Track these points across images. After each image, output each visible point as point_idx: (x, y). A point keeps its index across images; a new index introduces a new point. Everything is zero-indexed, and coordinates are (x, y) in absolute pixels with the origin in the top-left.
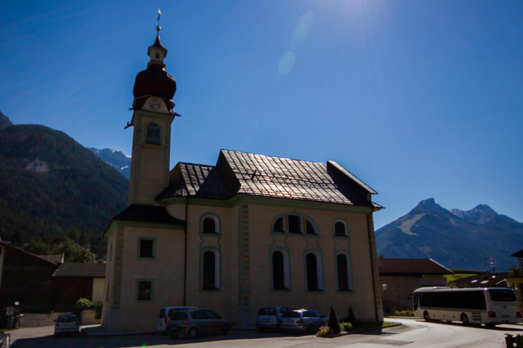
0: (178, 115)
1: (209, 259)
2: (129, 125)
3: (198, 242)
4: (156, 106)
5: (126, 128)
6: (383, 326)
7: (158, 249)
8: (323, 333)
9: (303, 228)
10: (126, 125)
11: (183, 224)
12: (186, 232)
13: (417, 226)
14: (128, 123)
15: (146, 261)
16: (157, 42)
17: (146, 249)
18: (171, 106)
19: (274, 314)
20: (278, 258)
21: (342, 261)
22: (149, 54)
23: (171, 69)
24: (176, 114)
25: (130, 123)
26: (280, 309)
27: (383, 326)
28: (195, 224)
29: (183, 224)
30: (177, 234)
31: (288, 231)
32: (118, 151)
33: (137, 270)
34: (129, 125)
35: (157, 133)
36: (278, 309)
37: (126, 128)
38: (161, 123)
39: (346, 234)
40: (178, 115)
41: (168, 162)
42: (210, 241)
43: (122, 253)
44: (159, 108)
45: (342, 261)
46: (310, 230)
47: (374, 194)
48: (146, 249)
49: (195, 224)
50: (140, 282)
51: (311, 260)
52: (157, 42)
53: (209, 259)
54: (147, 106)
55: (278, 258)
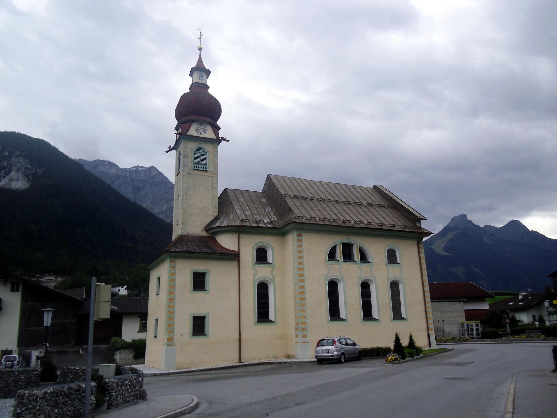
0: (225, 140)
1: (263, 290)
2: (170, 149)
3: (252, 273)
5: (167, 152)
6: (238, 251)
7: (211, 281)
9: (356, 256)
11: (234, 256)
14: (170, 147)
16: (200, 61)
18: (216, 129)
19: (333, 345)
20: (333, 286)
21: (394, 286)
22: (191, 75)
23: (216, 88)
24: (223, 139)
26: (339, 340)
27: (238, 251)
28: (248, 254)
33: (191, 304)
34: (170, 149)
36: (336, 339)
37: (167, 152)
39: (398, 261)
40: (225, 140)
41: (216, 189)
42: (263, 272)
43: (174, 287)
45: (394, 286)
46: (363, 258)
47: (423, 219)
51: (365, 287)
52: (200, 61)
53: (263, 290)
54: (193, 131)
55: (333, 286)
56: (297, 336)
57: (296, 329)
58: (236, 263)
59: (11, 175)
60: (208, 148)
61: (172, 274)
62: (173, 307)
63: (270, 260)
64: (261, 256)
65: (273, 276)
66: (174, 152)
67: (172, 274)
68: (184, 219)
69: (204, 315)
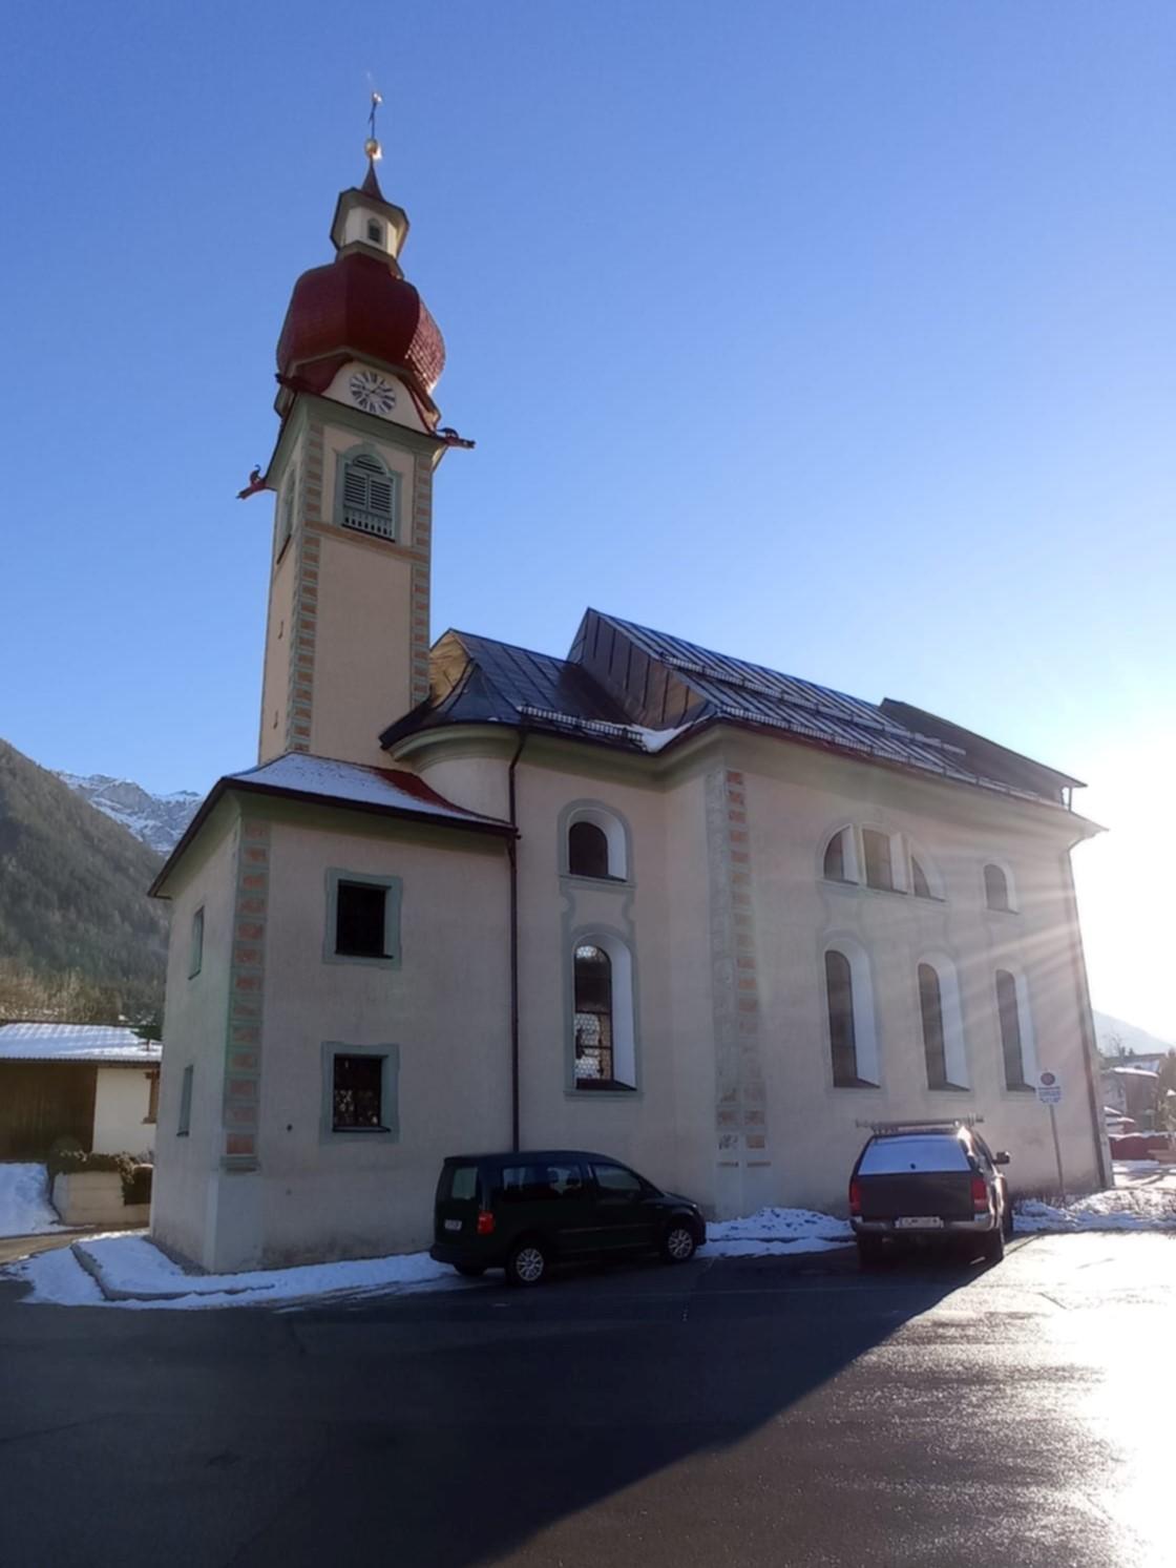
2: (259, 483)
4: (376, 400)
5: (244, 494)
7: (404, 920)
8: (1011, 1219)
10: (247, 484)
12: (513, 864)
13: (1028, 1480)
14: (254, 475)
15: (358, 971)
17: (361, 920)
25: (262, 475)
28: (544, 843)
29: (499, 837)
30: (482, 874)
31: (865, 880)
32: (129, 781)
34: (259, 483)
35: (382, 497)
37: (244, 494)
38: (396, 460)
42: (594, 902)
43: (259, 932)
44: (389, 407)
48: (361, 920)
49: (544, 843)
50: (339, 1060)
52: (371, 179)
54: (343, 387)
56: (725, 1143)
57: (724, 1117)
58: (505, 861)
59: (824, 1217)
60: (396, 460)
61: (736, 840)
62: (388, 486)
63: (617, 865)
64: (586, 851)
65: (631, 924)
66: (266, 499)
67: (736, 840)
68: (310, 491)
69: (382, 1053)
